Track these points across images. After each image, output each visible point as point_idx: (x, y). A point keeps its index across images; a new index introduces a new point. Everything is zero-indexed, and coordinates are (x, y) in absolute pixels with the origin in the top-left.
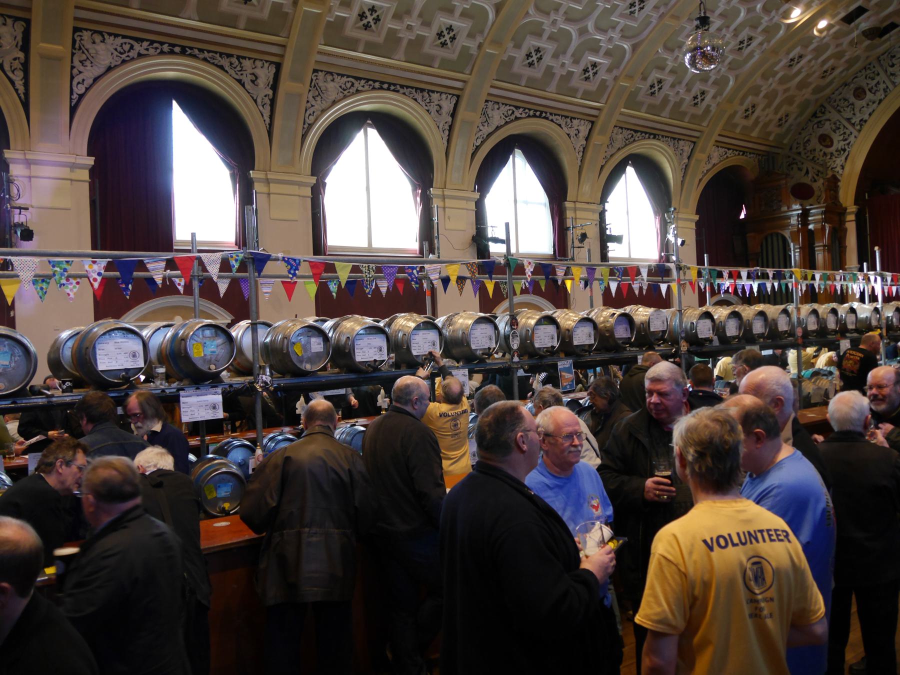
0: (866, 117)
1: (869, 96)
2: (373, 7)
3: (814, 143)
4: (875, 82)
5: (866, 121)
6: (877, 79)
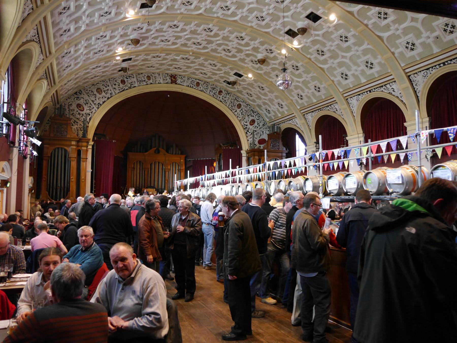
0: (101, 103)
1: (103, 94)
2: (455, 26)
3: (74, 106)
4: (106, 89)
5: (101, 105)
6: (108, 88)
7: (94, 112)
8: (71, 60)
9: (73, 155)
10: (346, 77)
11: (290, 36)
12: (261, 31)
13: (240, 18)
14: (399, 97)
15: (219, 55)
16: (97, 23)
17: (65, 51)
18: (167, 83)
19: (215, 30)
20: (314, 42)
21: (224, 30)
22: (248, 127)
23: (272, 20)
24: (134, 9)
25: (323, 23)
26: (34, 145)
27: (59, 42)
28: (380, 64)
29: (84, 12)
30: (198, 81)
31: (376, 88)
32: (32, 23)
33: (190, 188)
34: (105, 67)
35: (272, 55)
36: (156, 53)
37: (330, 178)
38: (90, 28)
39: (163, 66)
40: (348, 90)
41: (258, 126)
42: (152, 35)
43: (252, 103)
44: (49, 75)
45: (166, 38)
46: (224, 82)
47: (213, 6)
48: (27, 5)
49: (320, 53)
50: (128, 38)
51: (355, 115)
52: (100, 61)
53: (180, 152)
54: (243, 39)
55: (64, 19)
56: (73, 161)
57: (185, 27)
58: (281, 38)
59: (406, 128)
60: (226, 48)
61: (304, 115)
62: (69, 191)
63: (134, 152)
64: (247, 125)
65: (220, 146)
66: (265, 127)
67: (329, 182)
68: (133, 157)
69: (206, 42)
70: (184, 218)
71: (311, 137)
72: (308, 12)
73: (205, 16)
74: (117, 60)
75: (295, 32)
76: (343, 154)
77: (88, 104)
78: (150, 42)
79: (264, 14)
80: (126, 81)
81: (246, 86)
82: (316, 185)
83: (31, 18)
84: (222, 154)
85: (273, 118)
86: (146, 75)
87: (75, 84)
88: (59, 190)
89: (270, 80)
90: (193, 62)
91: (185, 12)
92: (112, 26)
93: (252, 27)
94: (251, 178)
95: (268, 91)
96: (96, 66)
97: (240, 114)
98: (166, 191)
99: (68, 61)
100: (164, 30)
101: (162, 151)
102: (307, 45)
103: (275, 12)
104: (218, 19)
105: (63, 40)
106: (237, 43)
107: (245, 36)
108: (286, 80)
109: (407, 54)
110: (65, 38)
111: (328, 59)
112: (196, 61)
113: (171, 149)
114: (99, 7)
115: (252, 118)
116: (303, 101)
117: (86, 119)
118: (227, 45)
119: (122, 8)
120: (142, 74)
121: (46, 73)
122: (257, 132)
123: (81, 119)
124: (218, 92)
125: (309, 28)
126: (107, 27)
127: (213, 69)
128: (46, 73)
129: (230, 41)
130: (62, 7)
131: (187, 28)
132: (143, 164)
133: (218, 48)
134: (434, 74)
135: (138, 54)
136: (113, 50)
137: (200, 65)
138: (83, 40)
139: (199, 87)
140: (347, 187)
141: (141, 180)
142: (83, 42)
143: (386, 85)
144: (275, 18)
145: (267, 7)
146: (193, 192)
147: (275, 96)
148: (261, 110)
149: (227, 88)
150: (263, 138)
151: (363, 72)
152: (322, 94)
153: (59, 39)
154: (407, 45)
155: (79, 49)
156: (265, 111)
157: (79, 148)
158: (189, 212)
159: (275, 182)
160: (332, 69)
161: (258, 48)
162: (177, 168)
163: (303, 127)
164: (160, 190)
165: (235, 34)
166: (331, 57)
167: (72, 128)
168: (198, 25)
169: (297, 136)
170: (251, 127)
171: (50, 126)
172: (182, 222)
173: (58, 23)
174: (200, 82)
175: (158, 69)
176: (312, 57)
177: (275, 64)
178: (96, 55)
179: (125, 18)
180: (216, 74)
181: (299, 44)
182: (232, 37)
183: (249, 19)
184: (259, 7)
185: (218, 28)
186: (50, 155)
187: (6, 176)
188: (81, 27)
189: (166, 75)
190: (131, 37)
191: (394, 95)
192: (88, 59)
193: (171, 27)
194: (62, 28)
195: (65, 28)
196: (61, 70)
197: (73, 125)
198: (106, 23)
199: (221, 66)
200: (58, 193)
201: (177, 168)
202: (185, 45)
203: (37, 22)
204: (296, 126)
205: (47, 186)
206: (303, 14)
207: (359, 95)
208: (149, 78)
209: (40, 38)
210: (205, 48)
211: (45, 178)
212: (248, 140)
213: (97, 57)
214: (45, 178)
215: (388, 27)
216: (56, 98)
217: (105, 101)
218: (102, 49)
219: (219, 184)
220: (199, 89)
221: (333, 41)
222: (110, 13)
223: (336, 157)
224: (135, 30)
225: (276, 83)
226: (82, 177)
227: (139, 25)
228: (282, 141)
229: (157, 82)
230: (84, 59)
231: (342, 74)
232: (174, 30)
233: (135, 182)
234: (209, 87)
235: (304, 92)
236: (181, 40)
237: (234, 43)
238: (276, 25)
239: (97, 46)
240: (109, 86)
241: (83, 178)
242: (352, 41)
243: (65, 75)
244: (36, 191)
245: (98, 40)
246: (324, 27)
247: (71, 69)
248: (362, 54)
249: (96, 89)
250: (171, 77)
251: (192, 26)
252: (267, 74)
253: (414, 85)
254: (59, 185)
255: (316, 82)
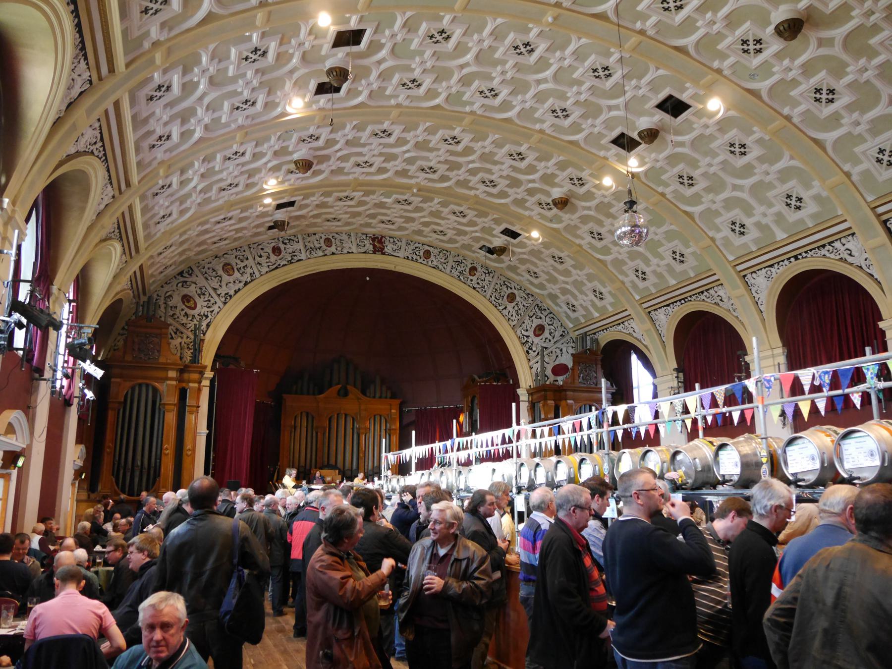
0: (232, 292)
1: (237, 275)
3: (176, 300)
4: (242, 265)
5: (231, 296)
6: (246, 262)
7: (216, 311)
8: (172, 203)
9: (170, 399)
10: (742, 230)
11: (623, 148)
14: (864, 267)
15: (472, 193)
16: (227, 125)
17: (161, 183)
18: (365, 252)
19: (466, 139)
20: (673, 159)
22: (530, 340)
23: (584, 116)
24: (304, 97)
25: (693, 119)
26: (88, 379)
27: (147, 160)
28: (817, 198)
29: (201, 98)
30: (428, 248)
31: (811, 250)
32: (89, 112)
33: (417, 469)
34: (241, 220)
35: (582, 190)
36: (345, 191)
37: (845, 436)
39: (358, 218)
40: (748, 256)
41: (551, 338)
42: (337, 151)
44: (124, 232)
45: (366, 159)
46: (481, 248)
48: (77, 71)
50: (289, 158)
51: (762, 308)
53: (389, 395)
55: (158, 111)
56: (169, 411)
57: (404, 135)
58: (602, 153)
59: (883, 333)
61: (649, 312)
62: (159, 475)
63: (296, 393)
64: (528, 337)
65: (474, 380)
66: (565, 339)
67: (788, 453)
68: (293, 403)
70: (442, 552)
72: (662, 96)
73: (446, 110)
74: (265, 206)
76: (827, 379)
78: (334, 168)
79: (568, 104)
80: (282, 249)
81: (525, 256)
82: (749, 459)
83: (88, 102)
84: (478, 396)
85: (583, 321)
87: (181, 254)
88: (137, 473)
89: (577, 241)
90: (418, 209)
91: (406, 103)
93: (541, 131)
95: (547, 280)
96: (223, 217)
97: (514, 314)
98: (361, 475)
99: (166, 204)
100: (362, 141)
101: (354, 392)
102: (658, 165)
104: (472, 117)
105: (155, 158)
107: (528, 152)
108: (636, 226)
109: (881, 174)
110: (160, 154)
111: (702, 193)
112: (425, 206)
113: (372, 387)
114: (230, 88)
115: (539, 322)
116: (646, 283)
117: (200, 326)
118: (489, 171)
119: (279, 93)
120: (315, 234)
121: (119, 228)
122: (550, 350)
123: (189, 326)
124: (468, 270)
127: (460, 223)
128: (119, 228)
129: (496, 163)
131: (409, 136)
132: (313, 418)
133: (470, 178)
134: (782, 274)
136: (257, 184)
137: (432, 214)
138: (198, 160)
139: (430, 261)
140: (847, 466)
142: (196, 164)
143: (833, 242)
147: (586, 275)
148: (557, 305)
149: (487, 261)
151: (779, 218)
152: (690, 268)
153: (147, 156)
154: (881, 156)
155: (189, 180)
156: (565, 308)
157: (184, 385)
158: (457, 535)
159: (631, 454)
160: (710, 214)
162: (383, 427)
164: (349, 473)
165: (507, 148)
166: (708, 190)
167: (169, 344)
168: (431, 131)
169: (634, 357)
170: (537, 340)
171: (125, 341)
172: (436, 562)
173: (146, 121)
174: (431, 249)
175: (348, 224)
176: (668, 191)
177: (589, 208)
178: (223, 193)
179: (284, 114)
181: (640, 166)
183: (536, 115)
184: (558, 88)
185: (472, 136)
186: (122, 400)
187: (16, 442)
189: (364, 237)
190: (296, 156)
191: (851, 264)
192: (207, 201)
195: (159, 131)
196: (152, 222)
197: (172, 338)
198: (246, 124)
199: (476, 216)
200: (136, 480)
201: (383, 427)
202: (403, 173)
203: (99, 112)
204: (632, 336)
205: (114, 464)
207: (772, 266)
208: (328, 242)
209: (106, 147)
211: (109, 447)
212: (531, 368)
213: (226, 198)
214: (109, 447)
215: (835, 120)
216: (139, 282)
217: (239, 290)
218: (235, 181)
219: (481, 460)
220: (430, 263)
222: (254, 103)
223: (807, 388)
224: (304, 141)
226: (188, 445)
227: (312, 130)
228: (603, 367)
229: (345, 251)
230: (199, 201)
231: (733, 223)
232: (382, 141)
233: (297, 455)
234: (450, 259)
235: (648, 265)
236: (397, 163)
237: (503, 167)
238: (593, 126)
239: (225, 173)
240: (247, 259)
242: (754, 152)
243: (158, 235)
244: (90, 477)
246: (695, 126)
247: (172, 223)
248: (778, 179)
250: (373, 240)
251: (420, 133)
253: (753, 292)
254: (139, 463)
255: (676, 242)
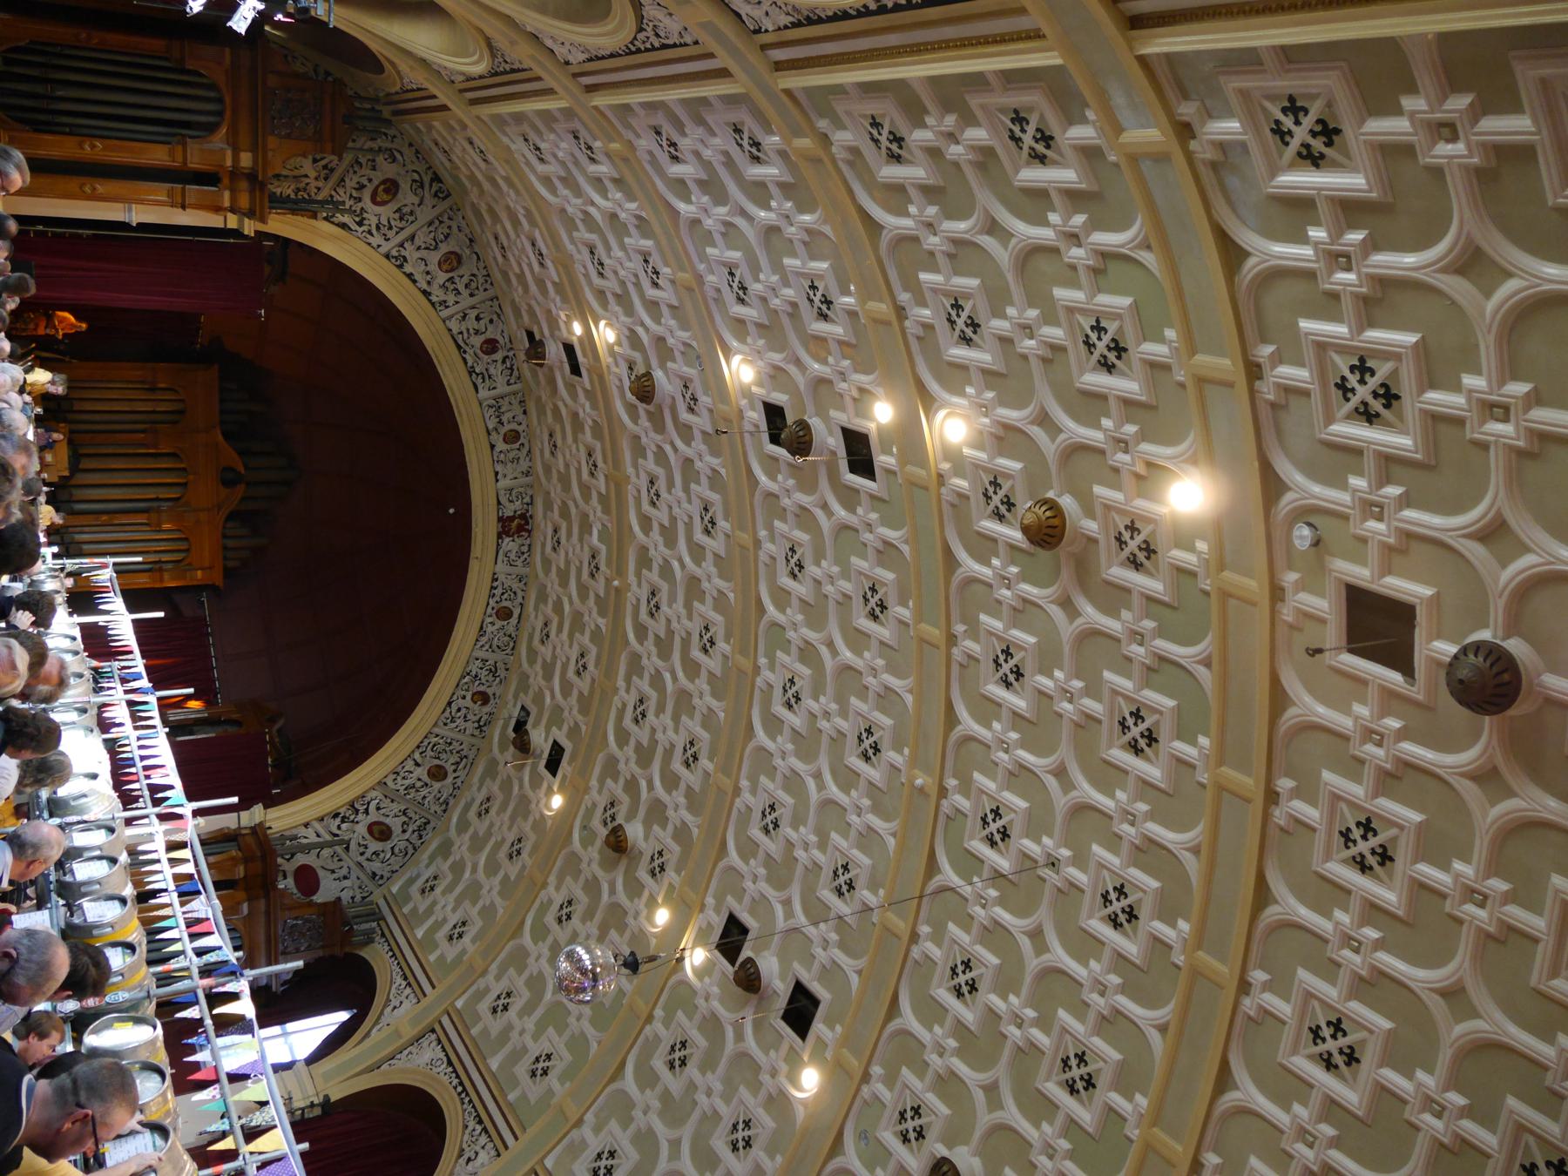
0: (408, 268)
1: (442, 277)
3: (387, 170)
4: (461, 287)
6: (465, 293)
7: (371, 240)
8: (563, 164)
9: (196, 156)
11: (724, 935)
12: (726, 829)
13: (762, 749)
15: (621, 683)
16: (703, 257)
17: (597, 144)
18: (499, 503)
19: (711, 663)
20: (712, 1026)
21: (714, 695)
23: (769, 860)
32: (707, 26)
33: (83, 627)
34: (541, 283)
35: (643, 874)
38: (684, 231)
42: (672, 444)
43: (455, 820)
44: (504, 80)
46: (523, 708)
47: (794, 650)
49: (677, 1055)
50: (654, 362)
52: (565, 267)
53: (231, 564)
54: (688, 765)
55: (717, 141)
56: (171, 154)
58: (710, 901)
60: (651, 706)
61: (433, 1031)
62: (36, 131)
64: (367, 812)
65: (273, 721)
66: (366, 881)
69: (662, 635)
71: (341, 1081)
72: (816, 988)
75: (738, 950)
77: (401, 219)
78: (644, 440)
79: (786, 830)
80: (495, 357)
81: (516, 789)
85: (406, 910)
86: (520, 429)
89: (552, 879)
90: (583, 591)
91: (763, 557)
92: (695, 305)
93: (737, 791)
94: (154, 894)
96: (544, 251)
97: (406, 782)
99: (560, 154)
103: (799, 870)
105: (638, 136)
106: (673, 746)
107: (700, 772)
108: (595, 979)
110: (646, 143)
111: (659, 1089)
112: (591, 602)
114: (764, 261)
115: (397, 829)
117: (343, 212)
118: (660, 709)
119: (761, 342)
120: (525, 412)
121: (513, 71)
122: (344, 856)
123: (341, 191)
124: (482, 688)
125: (761, 999)
126: (690, 289)
128: (513, 71)
130: (760, 136)
131: (709, 566)
132: (175, 423)
133: (646, 676)
135: (598, 397)
136: (606, 309)
138: (640, 208)
141: (106, 417)
142: (633, 206)
144: (780, 873)
145: (813, 838)
146: (67, 644)
148: (432, 858)
150: (323, 883)
153: (641, 121)
155: (603, 192)
157: (226, 181)
159: (153, 1042)
160: (623, 1108)
161: (664, 822)
162: (165, 557)
163: (384, 1034)
166: (666, 1096)
168: (720, 602)
169: (343, 1016)
170: (361, 829)
174: (514, 621)
175: (548, 469)
177: (612, 891)
178: (586, 252)
180: (548, 676)
182: (693, 726)
188: (689, 201)
189: (527, 499)
190: (658, 374)
192: (570, 225)
193: (706, 509)
194: (684, 134)
195: (685, 144)
196: (526, 128)
197: (315, 161)
199: (581, 693)
201: (165, 557)
202: (644, 561)
203: (711, 45)
204: (385, 1006)
206: (809, 971)
208: (512, 437)
210: (641, 632)
212: (306, 825)
213: (577, 256)
217: (414, 282)
218: (608, 272)
219: (112, 747)
221: (727, 1097)
224: (686, 387)
225: (580, 944)
226: (102, 187)
227: (704, 400)
229: (499, 468)
230: (570, 210)
232: (697, 520)
235: (521, 1014)
237: (670, 733)
239: (620, 254)
240: (472, 295)
241: (100, 189)
243: (505, 140)
245: (641, 258)
246: (772, 1053)
247: (528, 163)
249: (457, 249)
250: (523, 516)
251: (715, 583)
252: (573, 865)
254: (60, 93)
255: (568, 1057)
